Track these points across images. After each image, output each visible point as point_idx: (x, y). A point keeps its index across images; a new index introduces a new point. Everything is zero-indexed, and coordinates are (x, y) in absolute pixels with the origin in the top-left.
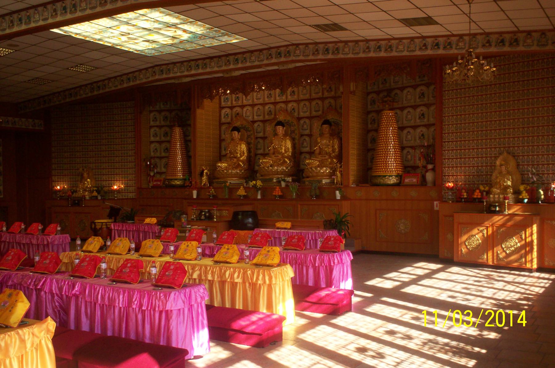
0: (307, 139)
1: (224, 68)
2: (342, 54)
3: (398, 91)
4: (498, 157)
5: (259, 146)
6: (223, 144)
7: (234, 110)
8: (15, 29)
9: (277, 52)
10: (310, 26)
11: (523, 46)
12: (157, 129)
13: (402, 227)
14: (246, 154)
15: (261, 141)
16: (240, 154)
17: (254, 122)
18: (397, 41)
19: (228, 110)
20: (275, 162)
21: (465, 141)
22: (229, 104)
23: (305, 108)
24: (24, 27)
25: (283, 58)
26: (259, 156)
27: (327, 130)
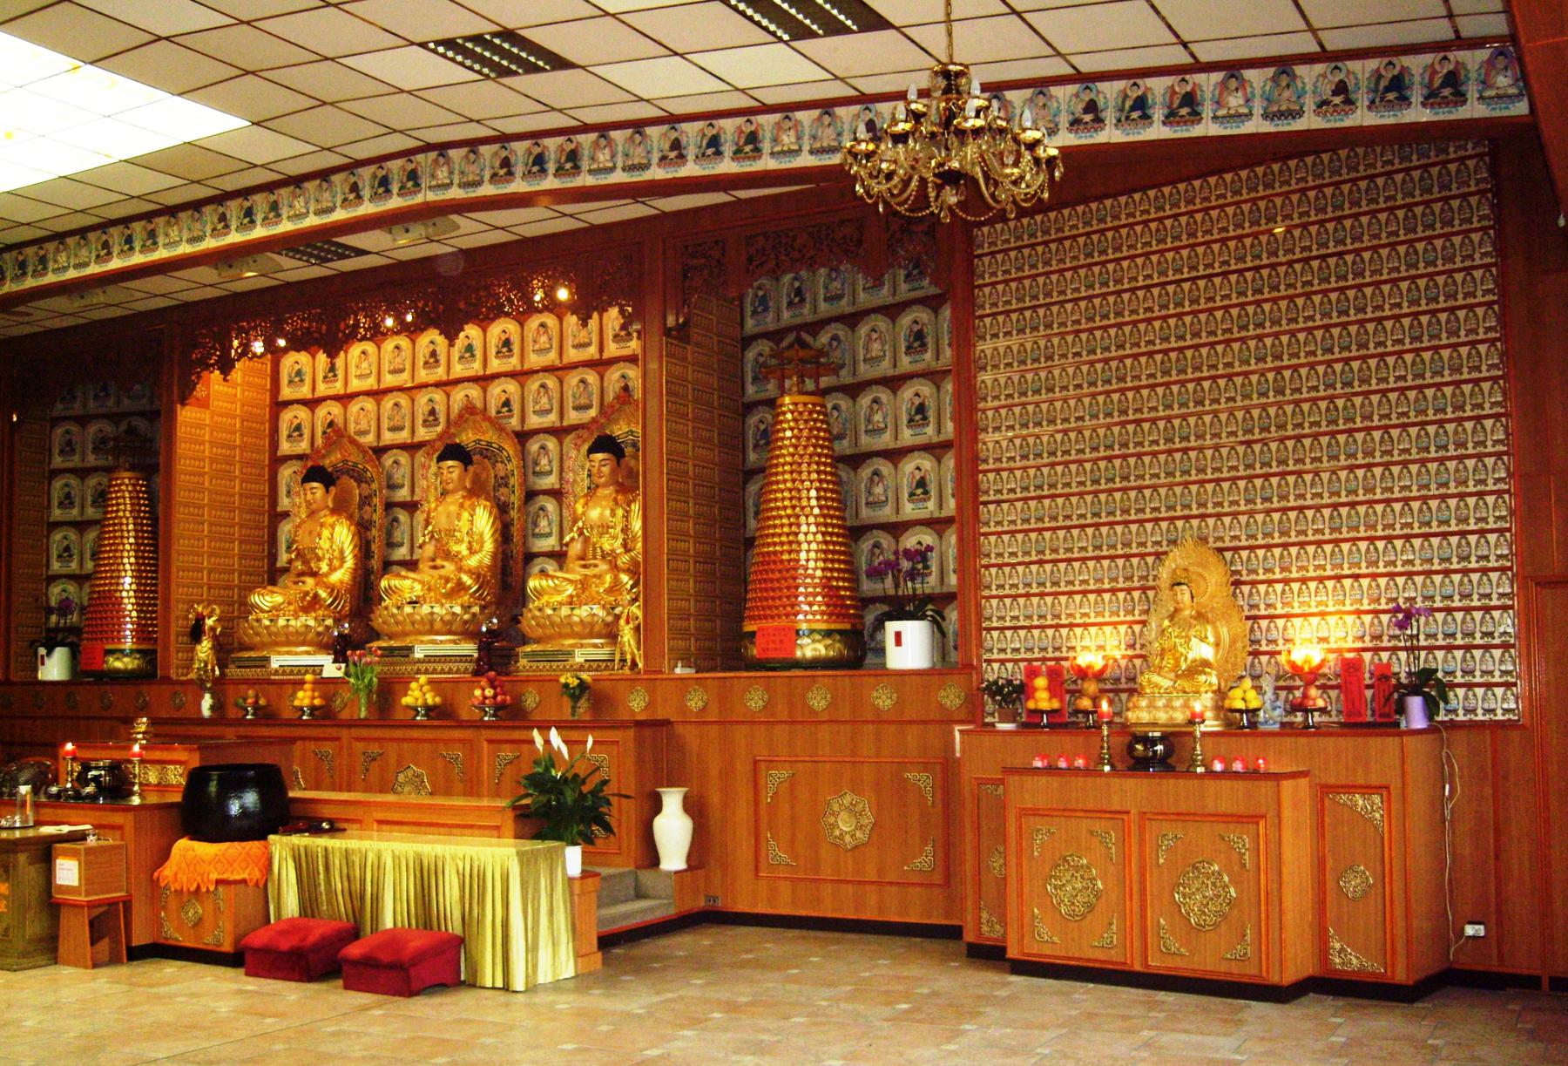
0: (550, 505)
1: (210, 243)
2: (590, 171)
3: (839, 330)
4: (1166, 553)
5: (397, 536)
6: (285, 529)
7: (321, 412)
8: (116, 264)
9: (374, 176)
10: (423, 45)
11: (1215, 118)
12: (74, 481)
13: (845, 824)
14: (350, 562)
15: (403, 516)
16: (330, 565)
17: (380, 451)
18: (777, 117)
19: (302, 413)
20: (430, 589)
21: (1203, 517)
22: (305, 392)
23: (544, 400)
24: (138, 259)
25: (395, 196)
26: (541, 559)
27: (606, 470)
